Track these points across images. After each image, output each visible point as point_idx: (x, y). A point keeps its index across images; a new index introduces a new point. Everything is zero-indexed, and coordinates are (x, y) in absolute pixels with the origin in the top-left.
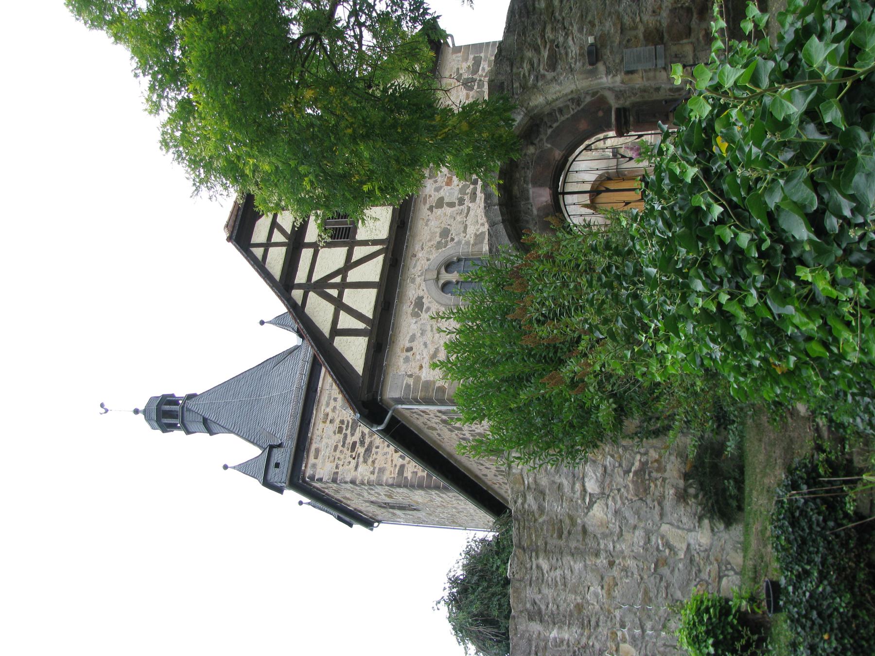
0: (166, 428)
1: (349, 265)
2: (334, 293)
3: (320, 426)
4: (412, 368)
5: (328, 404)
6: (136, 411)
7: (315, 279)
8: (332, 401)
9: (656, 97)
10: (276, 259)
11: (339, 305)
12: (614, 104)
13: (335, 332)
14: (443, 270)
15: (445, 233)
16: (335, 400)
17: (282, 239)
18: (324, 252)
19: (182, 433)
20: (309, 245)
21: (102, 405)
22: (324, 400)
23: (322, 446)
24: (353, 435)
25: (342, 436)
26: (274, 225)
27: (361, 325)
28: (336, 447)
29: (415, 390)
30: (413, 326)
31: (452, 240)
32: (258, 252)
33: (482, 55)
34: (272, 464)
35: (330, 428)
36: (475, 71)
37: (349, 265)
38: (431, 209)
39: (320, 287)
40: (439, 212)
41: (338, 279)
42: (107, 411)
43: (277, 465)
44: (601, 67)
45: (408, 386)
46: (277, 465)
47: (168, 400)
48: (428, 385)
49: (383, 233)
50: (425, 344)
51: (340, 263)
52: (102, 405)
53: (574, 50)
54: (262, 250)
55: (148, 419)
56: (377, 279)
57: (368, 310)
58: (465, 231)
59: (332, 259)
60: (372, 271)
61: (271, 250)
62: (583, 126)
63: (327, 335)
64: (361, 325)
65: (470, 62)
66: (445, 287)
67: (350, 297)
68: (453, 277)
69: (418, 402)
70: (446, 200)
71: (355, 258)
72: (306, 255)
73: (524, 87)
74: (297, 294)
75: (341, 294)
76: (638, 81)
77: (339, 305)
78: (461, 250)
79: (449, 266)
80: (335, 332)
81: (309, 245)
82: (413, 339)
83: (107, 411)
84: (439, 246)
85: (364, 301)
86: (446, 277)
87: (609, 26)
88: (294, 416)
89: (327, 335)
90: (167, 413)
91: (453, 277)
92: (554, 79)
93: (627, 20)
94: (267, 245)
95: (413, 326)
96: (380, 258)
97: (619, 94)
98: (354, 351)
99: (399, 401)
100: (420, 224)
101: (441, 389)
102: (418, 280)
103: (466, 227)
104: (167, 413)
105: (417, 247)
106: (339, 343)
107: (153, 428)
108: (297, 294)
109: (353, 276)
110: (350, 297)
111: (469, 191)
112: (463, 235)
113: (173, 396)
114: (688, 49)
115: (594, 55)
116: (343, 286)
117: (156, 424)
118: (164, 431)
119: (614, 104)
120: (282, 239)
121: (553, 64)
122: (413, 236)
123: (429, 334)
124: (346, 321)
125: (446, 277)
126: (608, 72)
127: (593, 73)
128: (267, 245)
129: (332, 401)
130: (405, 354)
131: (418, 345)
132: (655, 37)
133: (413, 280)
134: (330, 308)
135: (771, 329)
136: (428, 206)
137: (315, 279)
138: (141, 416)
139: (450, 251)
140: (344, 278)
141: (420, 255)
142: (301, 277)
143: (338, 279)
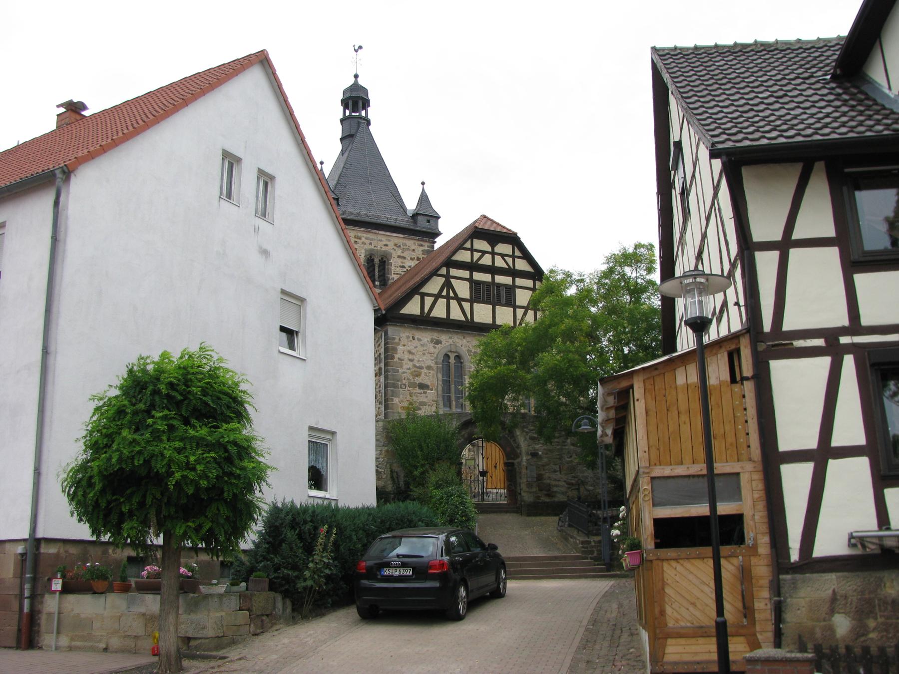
0: (345, 103)
1: (460, 300)
2: (444, 293)
4: (404, 340)
6: (356, 76)
7: (452, 280)
9: (518, 478)
10: (464, 256)
11: (437, 297)
12: (516, 462)
13: (423, 295)
16: (371, 244)
17: (475, 259)
18: (467, 284)
20: (471, 275)
21: (360, 47)
22: (370, 236)
26: (484, 253)
27: (426, 310)
29: (392, 343)
30: (426, 340)
32: (468, 245)
37: (460, 300)
39: (448, 285)
41: (452, 294)
42: (356, 51)
44: (529, 457)
45: (394, 339)
47: (366, 104)
48: (395, 350)
49: (477, 319)
50: (416, 347)
51: (460, 295)
52: (360, 47)
53: (537, 447)
57: (434, 314)
59: (463, 289)
60: (456, 314)
61: (469, 252)
62: (508, 449)
63: (422, 291)
64: (426, 310)
66: (447, 356)
67: (442, 302)
69: (385, 344)
71: (463, 303)
72: (466, 274)
73: (524, 427)
74: (444, 271)
75: (443, 297)
76: (524, 471)
77: (437, 297)
79: (458, 357)
80: (423, 295)
81: (471, 275)
82: (419, 340)
83: (356, 51)
85: (439, 312)
86: (452, 356)
87: (545, 460)
89: (422, 291)
92: (526, 439)
93: (547, 467)
94: (472, 250)
95: (426, 340)
96: (463, 319)
97: (520, 463)
98: (412, 308)
99: (386, 334)
101: (393, 357)
102: (451, 341)
105: (469, 339)
106: (417, 299)
107: (345, 92)
108: (444, 271)
109: (454, 304)
110: (442, 302)
113: (369, 106)
114: (534, 490)
115: (534, 455)
116: (448, 298)
117: (348, 95)
118: (342, 101)
119: (516, 462)
120: (475, 259)
121: (532, 438)
123: (422, 349)
124: (429, 301)
125: (452, 356)
126: (527, 460)
127: (527, 454)
128: (472, 250)
130: (411, 336)
131: (416, 343)
132: (540, 478)
133: (450, 338)
134: (436, 292)
135: (441, 503)
137: (452, 280)
140: (452, 298)
141: (464, 341)
142: (454, 272)
143: (452, 294)
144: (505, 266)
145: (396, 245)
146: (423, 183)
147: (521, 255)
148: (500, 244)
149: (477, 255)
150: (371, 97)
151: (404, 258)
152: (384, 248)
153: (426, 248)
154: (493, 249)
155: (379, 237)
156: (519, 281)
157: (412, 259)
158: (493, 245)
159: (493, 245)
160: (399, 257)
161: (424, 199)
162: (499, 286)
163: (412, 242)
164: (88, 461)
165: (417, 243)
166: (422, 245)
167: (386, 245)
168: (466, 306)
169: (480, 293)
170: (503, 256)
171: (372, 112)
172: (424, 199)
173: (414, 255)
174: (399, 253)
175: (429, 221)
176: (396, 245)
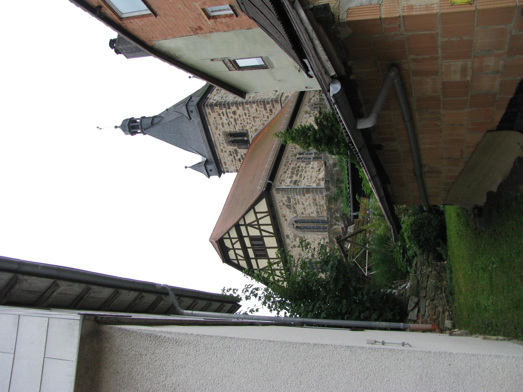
0: (133, 133)
2: (257, 227)
3: (221, 154)
5: (220, 146)
6: (116, 127)
8: (222, 145)
19: (142, 135)
21: (98, 127)
22: (218, 144)
23: (226, 160)
24: (237, 156)
25: (233, 157)
26: (236, 254)
28: (232, 161)
34: (190, 112)
35: (226, 155)
36: (290, 202)
42: (101, 129)
43: (192, 112)
47: (132, 121)
52: (98, 127)
55: (124, 130)
57: (272, 231)
65: (286, 198)
72: (253, 262)
88: (201, 131)
90: (132, 126)
91: (299, 225)
104: (132, 126)
107: (127, 134)
117: (128, 133)
129: (222, 145)
138: (120, 130)
145: (217, 129)
146: (186, 167)
149: (234, 241)
150: (129, 117)
151: (222, 123)
152: (222, 135)
153: (210, 110)
155: (216, 139)
156: (244, 233)
157: (221, 119)
158: (228, 249)
159: (228, 249)
160: (223, 126)
163: (210, 120)
165: (209, 117)
166: (209, 113)
167: (219, 135)
169: (261, 251)
171: (137, 116)
173: (218, 118)
175: (192, 112)
176: (217, 129)
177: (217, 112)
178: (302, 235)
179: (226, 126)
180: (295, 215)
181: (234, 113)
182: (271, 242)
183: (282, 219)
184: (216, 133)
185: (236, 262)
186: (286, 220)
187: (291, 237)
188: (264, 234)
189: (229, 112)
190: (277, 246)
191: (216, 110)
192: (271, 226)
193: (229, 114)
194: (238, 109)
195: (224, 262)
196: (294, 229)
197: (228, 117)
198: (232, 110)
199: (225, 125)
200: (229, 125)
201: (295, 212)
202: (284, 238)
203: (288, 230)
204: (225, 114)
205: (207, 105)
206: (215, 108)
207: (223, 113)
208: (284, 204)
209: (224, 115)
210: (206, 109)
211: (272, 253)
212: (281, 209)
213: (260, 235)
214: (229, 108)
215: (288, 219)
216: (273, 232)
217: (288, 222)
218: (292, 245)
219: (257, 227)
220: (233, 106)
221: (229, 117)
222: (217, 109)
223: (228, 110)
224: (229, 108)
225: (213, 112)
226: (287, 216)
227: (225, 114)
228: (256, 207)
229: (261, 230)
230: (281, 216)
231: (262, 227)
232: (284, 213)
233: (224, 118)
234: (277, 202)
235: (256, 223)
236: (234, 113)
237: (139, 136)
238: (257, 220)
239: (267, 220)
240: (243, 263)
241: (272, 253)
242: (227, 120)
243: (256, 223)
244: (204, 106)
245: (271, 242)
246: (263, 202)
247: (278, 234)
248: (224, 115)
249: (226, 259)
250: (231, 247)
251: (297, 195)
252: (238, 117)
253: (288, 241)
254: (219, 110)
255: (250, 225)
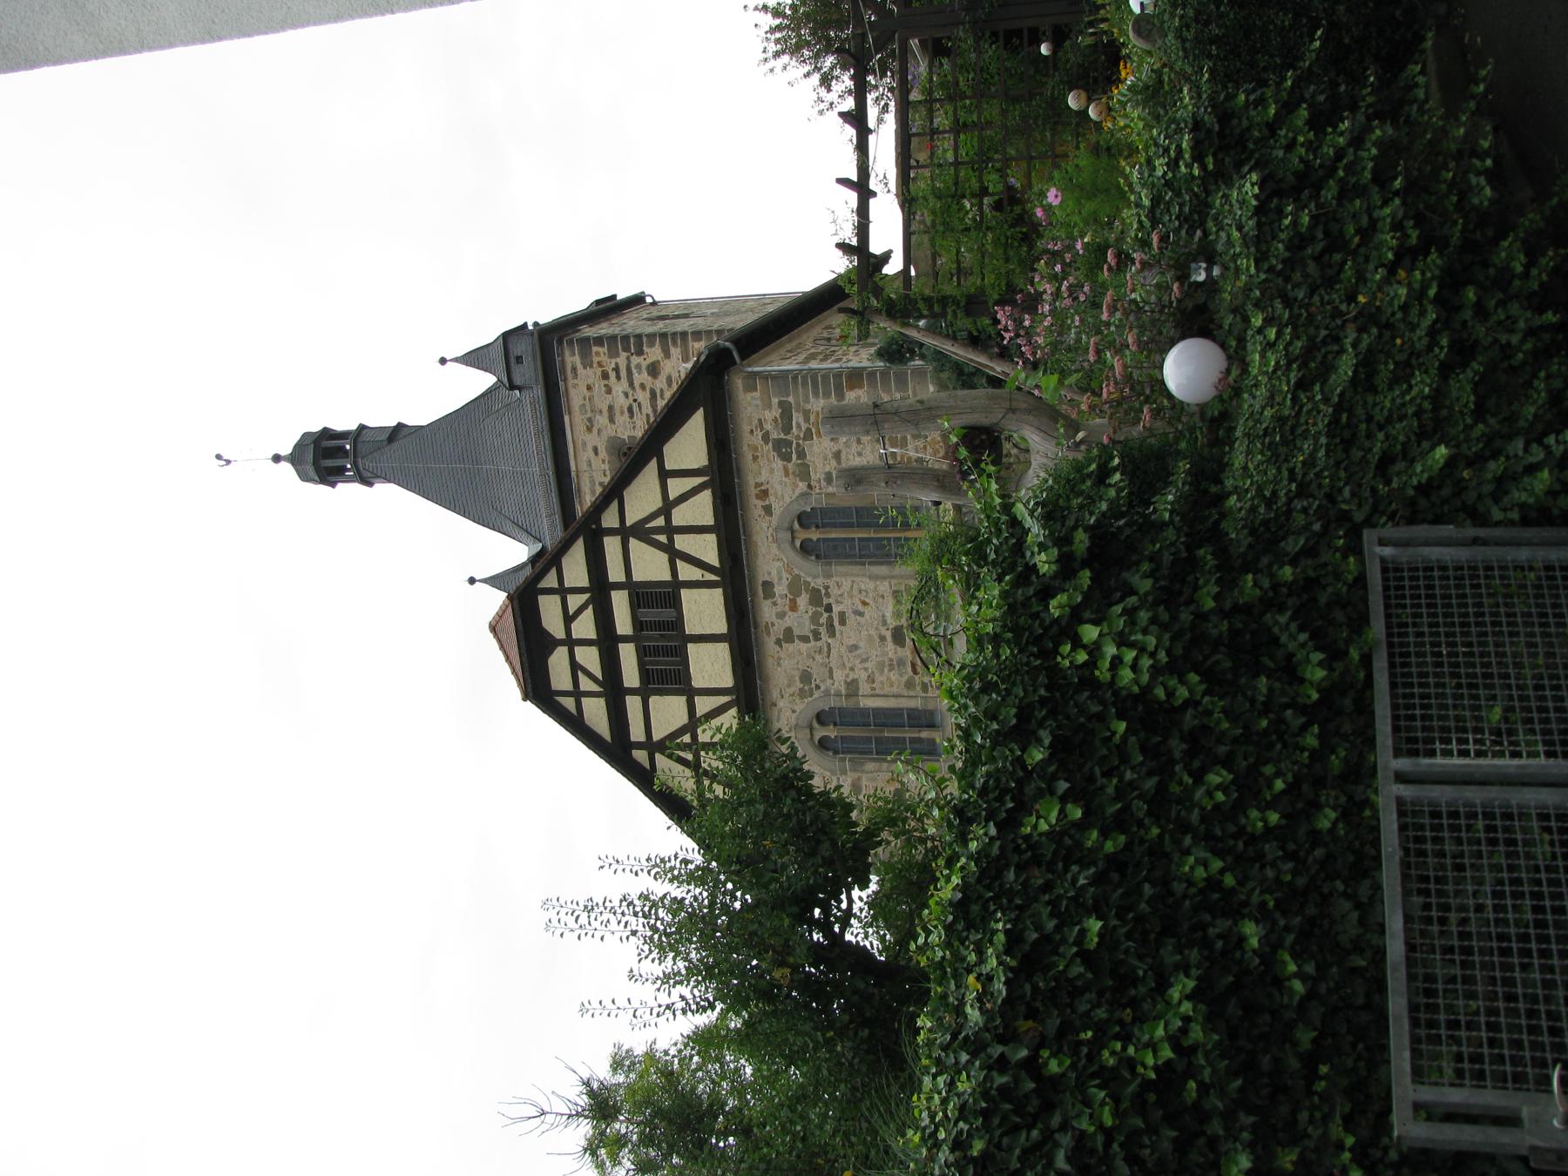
2: (663, 538)
6: (277, 458)
7: (657, 736)
14: (816, 725)
15: (806, 677)
17: (595, 688)
21: (219, 457)
26: (575, 667)
31: (818, 687)
33: (791, 399)
34: (513, 360)
36: (787, 428)
37: (694, 723)
38: (778, 642)
40: (790, 647)
42: (228, 462)
46: (519, 359)
51: (683, 719)
52: (219, 457)
54: (555, 585)
56: (711, 522)
57: (712, 558)
58: (831, 677)
65: (776, 412)
68: (831, 732)
70: (796, 632)
72: (633, 704)
78: (833, 702)
83: (583, 1009)
84: (802, 694)
90: (328, 457)
91: (831, 732)
100: (770, 662)
103: (831, 671)
104: (328, 457)
105: (775, 694)
111: (823, 620)
112: (829, 682)
122: (765, 680)
136: (774, 638)
138: (287, 468)
139: (818, 702)
141: (781, 704)
142: (637, 733)
144: (589, 611)
145: (589, 429)
147: (553, 572)
148: (545, 624)
149: (586, 684)
151: (611, 408)
152: (603, 454)
153: (577, 359)
154: (561, 643)
155: (584, 466)
156: (615, 573)
157: (609, 391)
158: (549, 644)
159: (549, 644)
160: (612, 420)
161: (474, 359)
162: (638, 624)
163: (572, 392)
164: (1117, 1109)
165: (571, 382)
166: (574, 369)
167: (596, 450)
168: (704, 705)
169: (666, 673)
170: (569, 619)
172: (474, 359)
173: (599, 386)
174: (602, 420)
175: (519, 359)
176: (589, 429)
177: (600, 364)
178: (818, 583)
179: (622, 419)
180: (802, 486)
181: (654, 370)
182: (704, 610)
183: (755, 506)
184: (584, 444)
185: (569, 703)
186: (768, 510)
187: (780, 589)
188: (687, 572)
189: (638, 366)
190: (711, 522)
191: (596, 359)
192: (718, 593)
193: (636, 375)
194: (667, 355)
195: (526, 697)
196: (792, 554)
197: (631, 384)
198: (649, 361)
199: (618, 417)
200: (632, 417)
201: (804, 473)
202: (754, 595)
203: (772, 560)
204: (623, 373)
205: (571, 342)
206: (595, 349)
207: (617, 370)
208: (766, 438)
209: (618, 378)
210: (567, 353)
211: (711, 666)
212: (755, 458)
213: (667, 577)
214: (640, 352)
215: (777, 508)
216: (715, 562)
217: (775, 520)
218: (778, 629)
219: (663, 538)
220: (651, 345)
221: (636, 384)
222: (600, 354)
223: (635, 360)
224: (640, 352)
225: (587, 364)
226: (774, 486)
227: (623, 373)
228: (668, 449)
229: (674, 555)
230: (752, 491)
231: (681, 542)
232: (762, 479)
233: (620, 388)
234: (746, 428)
235: (660, 522)
236: (654, 370)
237: (349, 492)
238: (667, 508)
239: (700, 509)
240: (596, 712)
241: (711, 666)
242: (626, 395)
243: (660, 522)
244: (560, 342)
245: (704, 610)
246: (696, 425)
247: (734, 575)
248: (618, 378)
249: (537, 689)
250: (560, 634)
251: (816, 394)
252: (665, 386)
253: (767, 612)
254: (604, 359)
255: (641, 531)
